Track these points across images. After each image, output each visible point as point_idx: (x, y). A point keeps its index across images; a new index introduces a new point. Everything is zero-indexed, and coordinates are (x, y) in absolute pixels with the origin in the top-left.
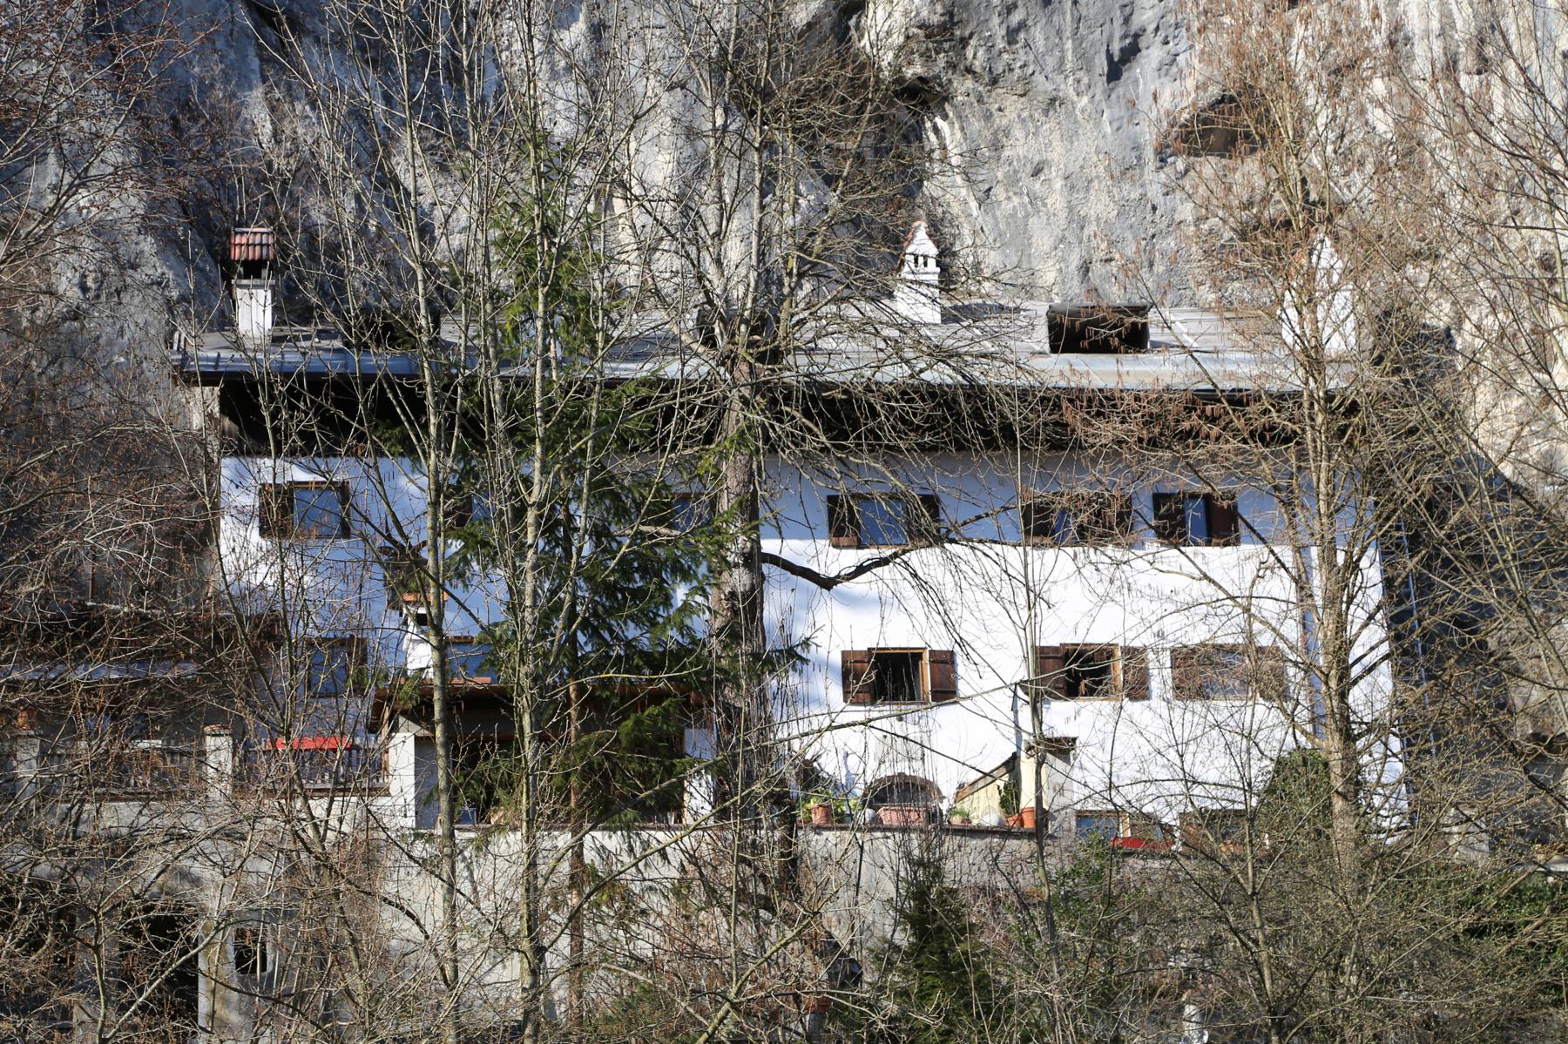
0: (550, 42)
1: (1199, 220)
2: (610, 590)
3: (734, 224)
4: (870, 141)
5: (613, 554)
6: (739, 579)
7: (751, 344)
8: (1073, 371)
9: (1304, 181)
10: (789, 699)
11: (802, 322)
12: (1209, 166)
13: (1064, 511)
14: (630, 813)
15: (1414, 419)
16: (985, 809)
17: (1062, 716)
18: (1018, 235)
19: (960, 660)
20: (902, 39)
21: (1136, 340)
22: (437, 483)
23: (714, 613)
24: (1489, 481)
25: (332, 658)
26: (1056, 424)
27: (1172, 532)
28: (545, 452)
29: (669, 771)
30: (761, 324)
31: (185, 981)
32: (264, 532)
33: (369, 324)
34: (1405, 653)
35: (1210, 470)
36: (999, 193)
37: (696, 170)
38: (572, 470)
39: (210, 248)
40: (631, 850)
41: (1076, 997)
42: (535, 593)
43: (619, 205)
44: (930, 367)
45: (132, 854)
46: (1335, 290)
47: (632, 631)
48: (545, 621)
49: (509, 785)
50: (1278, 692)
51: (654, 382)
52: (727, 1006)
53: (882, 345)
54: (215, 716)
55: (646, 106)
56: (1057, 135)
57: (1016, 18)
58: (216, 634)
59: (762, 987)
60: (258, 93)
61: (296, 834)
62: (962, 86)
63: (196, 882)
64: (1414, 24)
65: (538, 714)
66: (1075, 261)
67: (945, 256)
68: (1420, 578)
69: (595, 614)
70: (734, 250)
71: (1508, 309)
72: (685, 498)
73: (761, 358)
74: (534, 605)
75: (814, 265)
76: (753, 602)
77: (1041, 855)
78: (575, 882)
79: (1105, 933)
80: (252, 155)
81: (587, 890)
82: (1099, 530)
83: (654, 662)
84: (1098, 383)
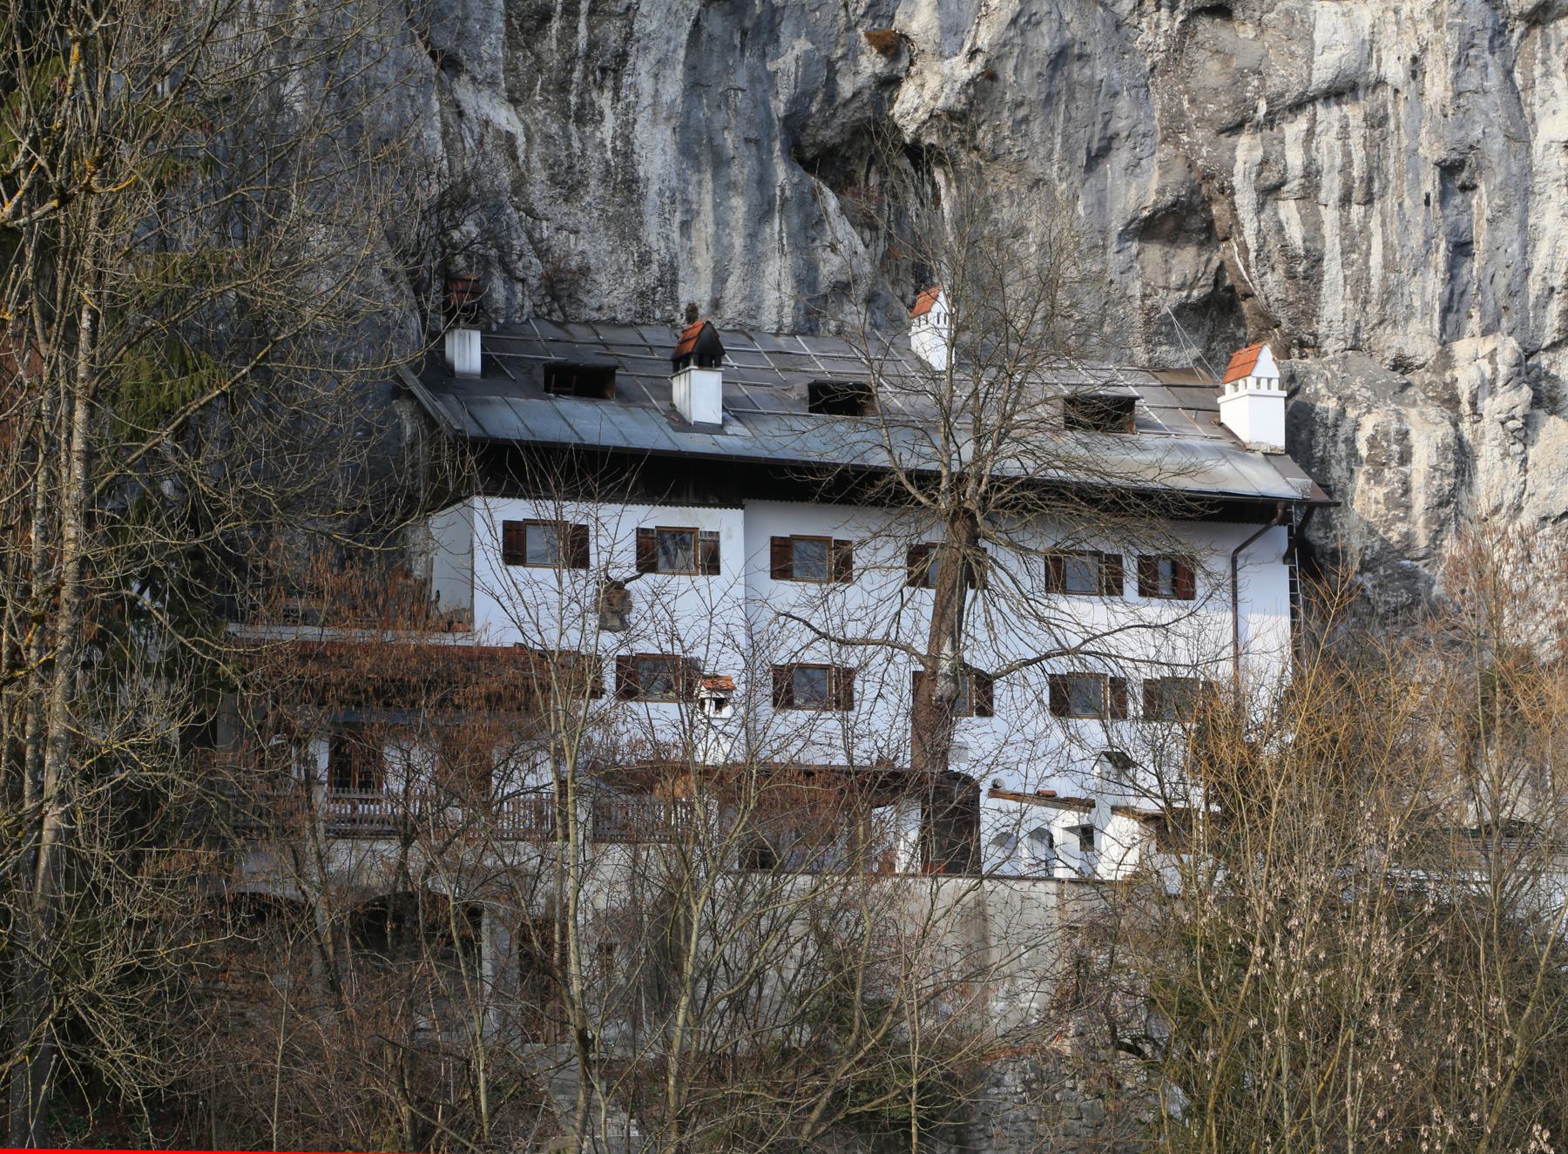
12: (1154, 252)
20: (926, 116)
57: (1021, 113)
64: (1323, 160)
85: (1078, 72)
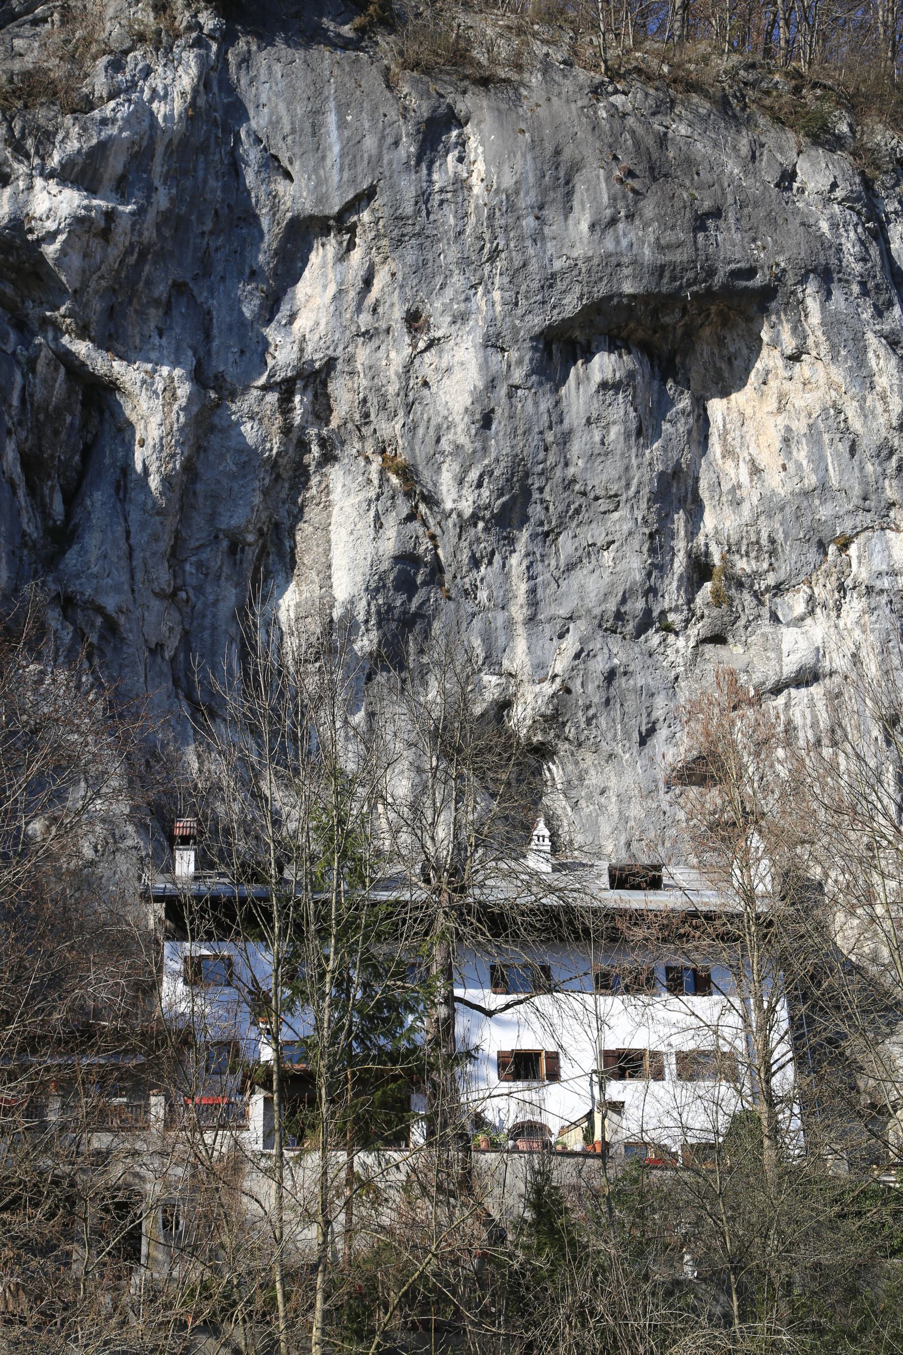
0: (346, 722)
1: (687, 821)
2: (371, 1018)
3: (442, 818)
4: (513, 776)
5: (373, 998)
6: (442, 1011)
7: (449, 883)
8: (621, 900)
9: (742, 802)
10: (470, 1079)
11: (477, 871)
12: (693, 791)
13: (617, 976)
14: (379, 1144)
15: (802, 931)
16: (575, 1141)
17: (616, 1090)
18: (593, 826)
19: (561, 1057)
21: (655, 884)
22: (278, 959)
23: (427, 1032)
24: (843, 964)
25: (219, 1054)
26: (613, 928)
27: (676, 987)
28: (337, 942)
29: (401, 1120)
30: (455, 872)
31: (134, 1237)
32: (186, 982)
33: (244, 872)
34: (801, 1058)
35: (695, 956)
36: (583, 803)
37: (421, 790)
38: (352, 952)
39: (163, 829)
40: (380, 1164)
41: (623, 1252)
42: (329, 1020)
43: (380, 808)
44: (546, 896)
45: (106, 1166)
46: (759, 860)
47: (382, 1041)
48: (334, 1036)
49: (313, 1127)
50: (733, 1077)
51: (397, 903)
52: (430, 1256)
53: (520, 884)
54: (153, 1086)
55: (395, 757)
56: (613, 773)
57: (591, 712)
58: (157, 1042)
59: (450, 1245)
60: (192, 747)
61: (196, 1155)
62: (563, 747)
63: (142, 1178)
64: (798, 721)
65: (330, 1088)
66: (623, 840)
67: (554, 836)
68: (808, 1017)
69: (362, 1031)
70: (441, 833)
71: (851, 873)
72: (413, 965)
73: (455, 890)
74: (329, 1027)
75: (484, 841)
76: (448, 1024)
77: (604, 1167)
78: (349, 1183)
79: (640, 1214)
80: (186, 780)
81: (355, 1187)
82: (636, 987)
83: (394, 1057)
84: (635, 905)
85: (621, 682)
